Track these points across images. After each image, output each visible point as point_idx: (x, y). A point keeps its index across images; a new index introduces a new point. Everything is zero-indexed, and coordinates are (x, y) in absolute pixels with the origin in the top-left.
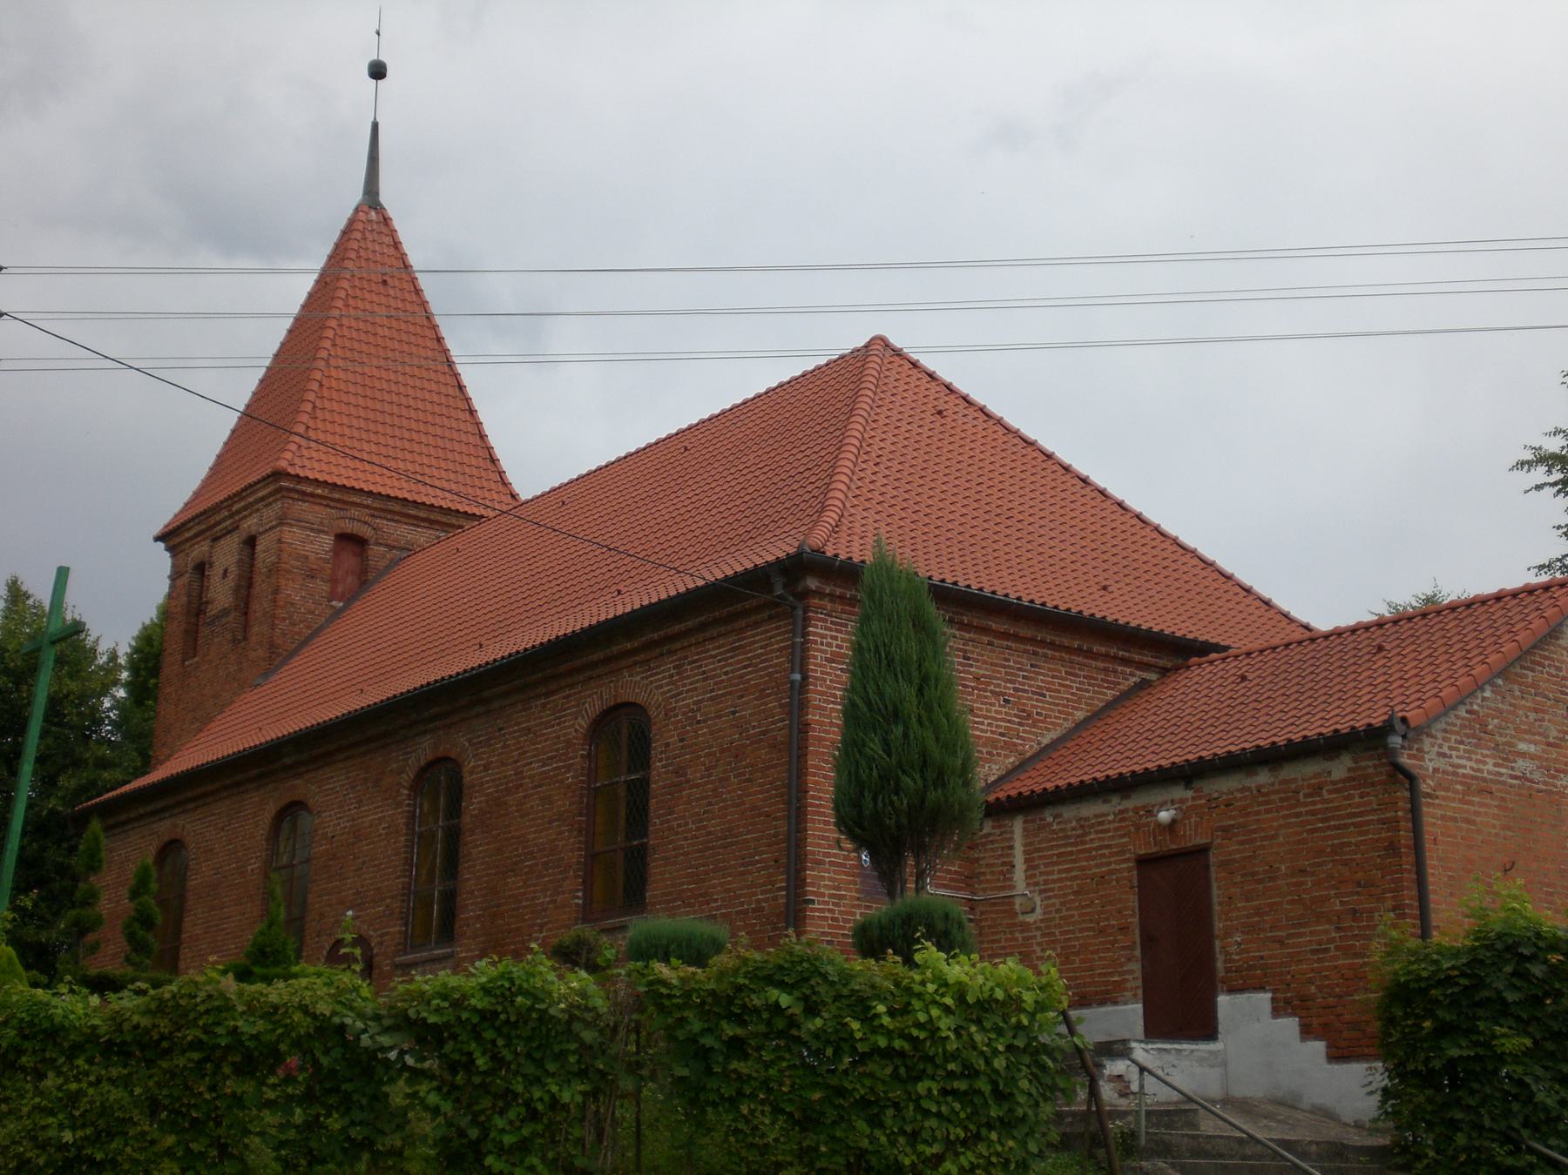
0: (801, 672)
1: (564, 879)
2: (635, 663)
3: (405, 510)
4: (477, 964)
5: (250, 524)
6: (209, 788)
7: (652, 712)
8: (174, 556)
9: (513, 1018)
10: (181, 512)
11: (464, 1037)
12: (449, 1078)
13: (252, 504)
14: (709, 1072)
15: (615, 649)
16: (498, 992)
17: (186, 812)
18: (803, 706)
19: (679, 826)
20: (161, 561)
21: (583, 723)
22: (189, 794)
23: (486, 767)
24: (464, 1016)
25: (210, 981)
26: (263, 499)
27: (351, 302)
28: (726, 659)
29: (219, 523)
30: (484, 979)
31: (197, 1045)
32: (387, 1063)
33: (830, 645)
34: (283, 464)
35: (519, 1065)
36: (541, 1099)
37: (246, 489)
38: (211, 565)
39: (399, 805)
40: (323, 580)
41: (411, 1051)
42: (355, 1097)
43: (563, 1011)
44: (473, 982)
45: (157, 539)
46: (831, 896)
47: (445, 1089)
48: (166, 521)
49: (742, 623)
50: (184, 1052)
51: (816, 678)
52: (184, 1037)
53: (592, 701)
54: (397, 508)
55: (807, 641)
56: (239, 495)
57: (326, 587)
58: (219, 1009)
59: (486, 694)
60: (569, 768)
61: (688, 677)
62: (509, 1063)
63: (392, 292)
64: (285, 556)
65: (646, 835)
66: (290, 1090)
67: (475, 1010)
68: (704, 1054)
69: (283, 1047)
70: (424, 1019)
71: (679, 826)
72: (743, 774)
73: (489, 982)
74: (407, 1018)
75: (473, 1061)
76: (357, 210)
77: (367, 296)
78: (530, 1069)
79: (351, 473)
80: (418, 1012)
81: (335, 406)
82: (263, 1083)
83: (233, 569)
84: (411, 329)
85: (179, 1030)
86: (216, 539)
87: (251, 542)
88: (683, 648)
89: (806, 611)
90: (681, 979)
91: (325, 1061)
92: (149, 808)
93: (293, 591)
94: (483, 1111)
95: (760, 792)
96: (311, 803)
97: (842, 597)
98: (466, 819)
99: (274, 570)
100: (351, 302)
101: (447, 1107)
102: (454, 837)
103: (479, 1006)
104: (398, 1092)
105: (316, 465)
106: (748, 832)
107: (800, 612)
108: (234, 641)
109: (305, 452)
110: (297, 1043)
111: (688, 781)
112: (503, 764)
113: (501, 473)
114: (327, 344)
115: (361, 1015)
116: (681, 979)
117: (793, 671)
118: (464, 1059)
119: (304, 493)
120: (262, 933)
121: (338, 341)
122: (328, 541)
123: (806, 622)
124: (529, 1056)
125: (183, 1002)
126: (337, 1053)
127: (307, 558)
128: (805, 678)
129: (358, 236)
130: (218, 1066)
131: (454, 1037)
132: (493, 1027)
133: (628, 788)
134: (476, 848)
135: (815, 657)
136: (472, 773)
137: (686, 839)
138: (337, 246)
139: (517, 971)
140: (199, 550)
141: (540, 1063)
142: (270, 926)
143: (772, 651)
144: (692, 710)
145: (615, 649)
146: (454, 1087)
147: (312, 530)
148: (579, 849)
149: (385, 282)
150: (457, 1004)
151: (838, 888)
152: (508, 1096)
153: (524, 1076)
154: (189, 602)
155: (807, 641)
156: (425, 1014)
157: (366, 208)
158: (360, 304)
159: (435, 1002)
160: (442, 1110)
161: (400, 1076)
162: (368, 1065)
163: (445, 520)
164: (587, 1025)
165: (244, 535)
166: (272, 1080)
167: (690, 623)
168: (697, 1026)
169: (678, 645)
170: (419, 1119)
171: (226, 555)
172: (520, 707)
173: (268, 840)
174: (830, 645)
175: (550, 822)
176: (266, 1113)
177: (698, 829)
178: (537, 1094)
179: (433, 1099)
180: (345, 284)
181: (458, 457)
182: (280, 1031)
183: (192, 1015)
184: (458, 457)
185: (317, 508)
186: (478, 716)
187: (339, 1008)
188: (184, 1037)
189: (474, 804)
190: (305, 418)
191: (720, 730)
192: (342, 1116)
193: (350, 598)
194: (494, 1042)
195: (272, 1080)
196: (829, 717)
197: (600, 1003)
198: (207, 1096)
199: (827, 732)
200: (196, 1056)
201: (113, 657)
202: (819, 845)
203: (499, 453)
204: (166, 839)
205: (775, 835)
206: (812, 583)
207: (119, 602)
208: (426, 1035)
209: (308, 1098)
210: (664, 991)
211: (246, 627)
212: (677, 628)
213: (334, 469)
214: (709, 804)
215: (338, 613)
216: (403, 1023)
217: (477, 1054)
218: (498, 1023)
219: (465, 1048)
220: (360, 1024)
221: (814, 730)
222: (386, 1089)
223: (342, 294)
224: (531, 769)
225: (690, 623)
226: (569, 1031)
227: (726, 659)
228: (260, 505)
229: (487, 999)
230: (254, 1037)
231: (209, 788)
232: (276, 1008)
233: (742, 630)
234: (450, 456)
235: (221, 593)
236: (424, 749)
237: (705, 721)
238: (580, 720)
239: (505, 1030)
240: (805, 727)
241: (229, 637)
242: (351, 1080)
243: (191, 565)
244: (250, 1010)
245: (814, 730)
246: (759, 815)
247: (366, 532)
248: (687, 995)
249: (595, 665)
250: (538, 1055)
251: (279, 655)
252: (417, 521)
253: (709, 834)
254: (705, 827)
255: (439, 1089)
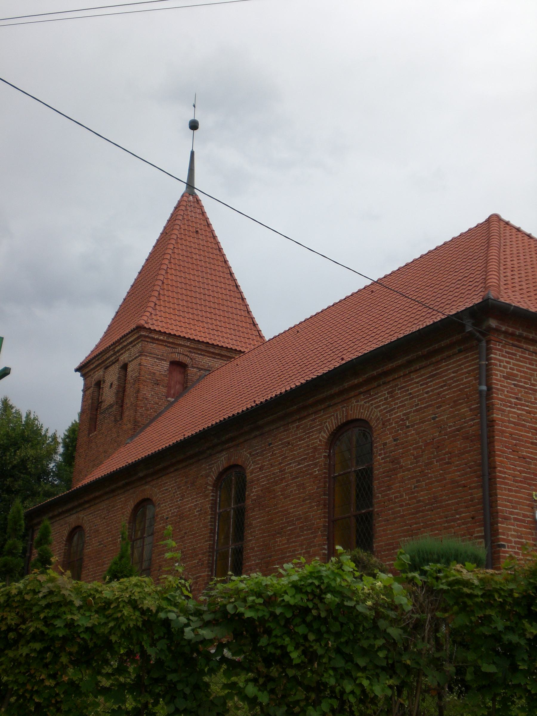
0: (487, 385)
1: (315, 537)
2: (360, 393)
3: (208, 349)
4: (285, 566)
5: (124, 357)
6: (97, 494)
7: (373, 424)
8: (85, 379)
9: (323, 615)
10: (89, 355)
11: (277, 632)
12: (264, 670)
13: (125, 346)
14: (514, 668)
15: (346, 385)
16: (309, 589)
17: (85, 509)
18: (490, 408)
19: (396, 497)
20: (79, 381)
21: (324, 435)
22: (86, 499)
23: (261, 469)
24: (278, 611)
25: (52, 580)
26: (131, 343)
27: (179, 241)
28: (426, 383)
29: (108, 358)
30: (295, 578)
31: (38, 636)
32: (208, 657)
33: (505, 367)
34: (143, 322)
35: (330, 659)
36: (352, 692)
37: (123, 337)
38: (104, 382)
39: (207, 496)
40: (163, 386)
41: (227, 645)
42: (180, 687)
43: (370, 608)
44: (284, 581)
45: (77, 370)
46: (516, 542)
47: (261, 681)
48: (81, 361)
49: (439, 357)
50: (28, 642)
51: (498, 389)
52: (27, 629)
53: (331, 421)
54: (203, 348)
55: (491, 364)
56: (118, 342)
57: (165, 390)
58: (59, 604)
59: (261, 422)
60: (316, 465)
61: (399, 398)
62: (322, 656)
63: (201, 237)
64: (142, 373)
65: (372, 505)
66: (122, 679)
67: (288, 606)
68: (510, 651)
69: (114, 638)
70: (242, 614)
71: (396, 497)
72: (444, 459)
73: (300, 580)
74: (225, 612)
75: (286, 654)
76: (183, 196)
77: (188, 238)
78: (340, 663)
79: (179, 329)
80: (235, 607)
81: (170, 294)
82: (99, 673)
83: (116, 383)
84: (211, 256)
85: (24, 623)
86: (107, 368)
87: (125, 367)
88: (394, 379)
89: (488, 342)
90: (481, 580)
91: (151, 651)
92: (65, 508)
93: (147, 392)
94: (297, 702)
95: (458, 470)
96: (154, 499)
97: (512, 334)
98: (249, 502)
99: (137, 380)
100: (179, 241)
101: (264, 698)
102: (241, 513)
103: (292, 602)
104: (217, 683)
105: (160, 324)
106: (450, 499)
107: (484, 344)
108: (116, 421)
109: (154, 317)
110: (127, 635)
111: (401, 467)
112: (272, 466)
113: (259, 331)
114: (167, 262)
115: (185, 611)
116: (481, 580)
117: (480, 384)
118: (278, 652)
119: (153, 339)
120: (115, 563)
121: (172, 261)
122: (166, 365)
123: (489, 350)
124: (338, 651)
125: (27, 597)
126: (162, 644)
127: (154, 373)
128: (490, 389)
129: (184, 208)
130: (56, 656)
131: (268, 632)
132: (304, 621)
133: (357, 475)
134: (256, 520)
135: (496, 375)
136: (252, 473)
137: (401, 506)
138: (172, 215)
139: (325, 570)
140: (98, 374)
141: (349, 659)
142: (121, 557)
143: (462, 374)
144: (402, 420)
145: (346, 385)
146: (269, 679)
147: (158, 359)
148: (325, 517)
149: (197, 232)
150: (269, 602)
151: (521, 537)
152: (320, 688)
153: (335, 669)
154: (92, 403)
155: (491, 364)
156: (241, 610)
157: (188, 195)
158: (184, 242)
159: (251, 598)
160: (260, 700)
161: (219, 667)
162: (189, 657)
163: (228, 354)
164: (394, 622)
165: (122, 364)
166: (107, 670)
167: (400, 362)
168: (500, 624)
169: (390, 378)
170: (237, 708)
171: (112, 376)
172: (282, 429)
173: (129, 523)
174: (505, 367)
175: (303, 501)
176: (101, 699)
177: (410, 499)
178: (349, 688)
179: (251, 690)
180: (176, 232)
181: (236, 322)
182: (111, 624)
183: (35, 609)
184: (236, 322)
185: (160, 347)
186: (255, 437)
187: (164, 604)
188: (27, 629)
189: (253, 493)
190: (154, 299)
191: (424, 431)
192: (167, 704)
193: (178, 396)
194: (305, 637)
195: (107, 670)
196: (507, 416)
197: (404, 600)
198: (47, 683)
199: (507, 427)
200: (38, 646)
201: (54, 438)
202: (506, 506)
203: (257, 321)
204: (73, 525)
205: (472, 500)
206: (493, 323)
207: (53, 400)
208: (243, 630)
209: (138, 687)
210: (466, 590)
211: (122, 414)
212: (390, 366)
213: (169, 326)
214: (418, 481)
215: (171, 404)
216: (223, 618)
217: (290, 648)
218: (309, 619)
219: (279, 642)
220: (183, 620)
221: (498, 425)
222: (206, 679)
223: (175, 237)
224: (291, 469)
225: (400, 362)
226: (375, 627)
227: (426, 383)
228: (130, 346)
229: (299, 596)
230: (90, 630)
231: (97, 494)
232: (108, 603)
233: (438, 362)
234: (231, 321)
235: (109, 396)
236: (222, 461)
237: (413, 426)
238: (322, 433)
239: (315, 626)
240: (491, 423)
241: (113, 419)
242: (175, 671)
243: (93, 383)
244: (86, 606)
245: (498, 425)
246: (459, 486)
247: (186, 360)
248: (488, 594)
249: (332, 397)
250: (347, 650)
251: (139, 426)
252: (214, 355)
253: (419, 501)
254: (415, 497)
255: (255, 680)
